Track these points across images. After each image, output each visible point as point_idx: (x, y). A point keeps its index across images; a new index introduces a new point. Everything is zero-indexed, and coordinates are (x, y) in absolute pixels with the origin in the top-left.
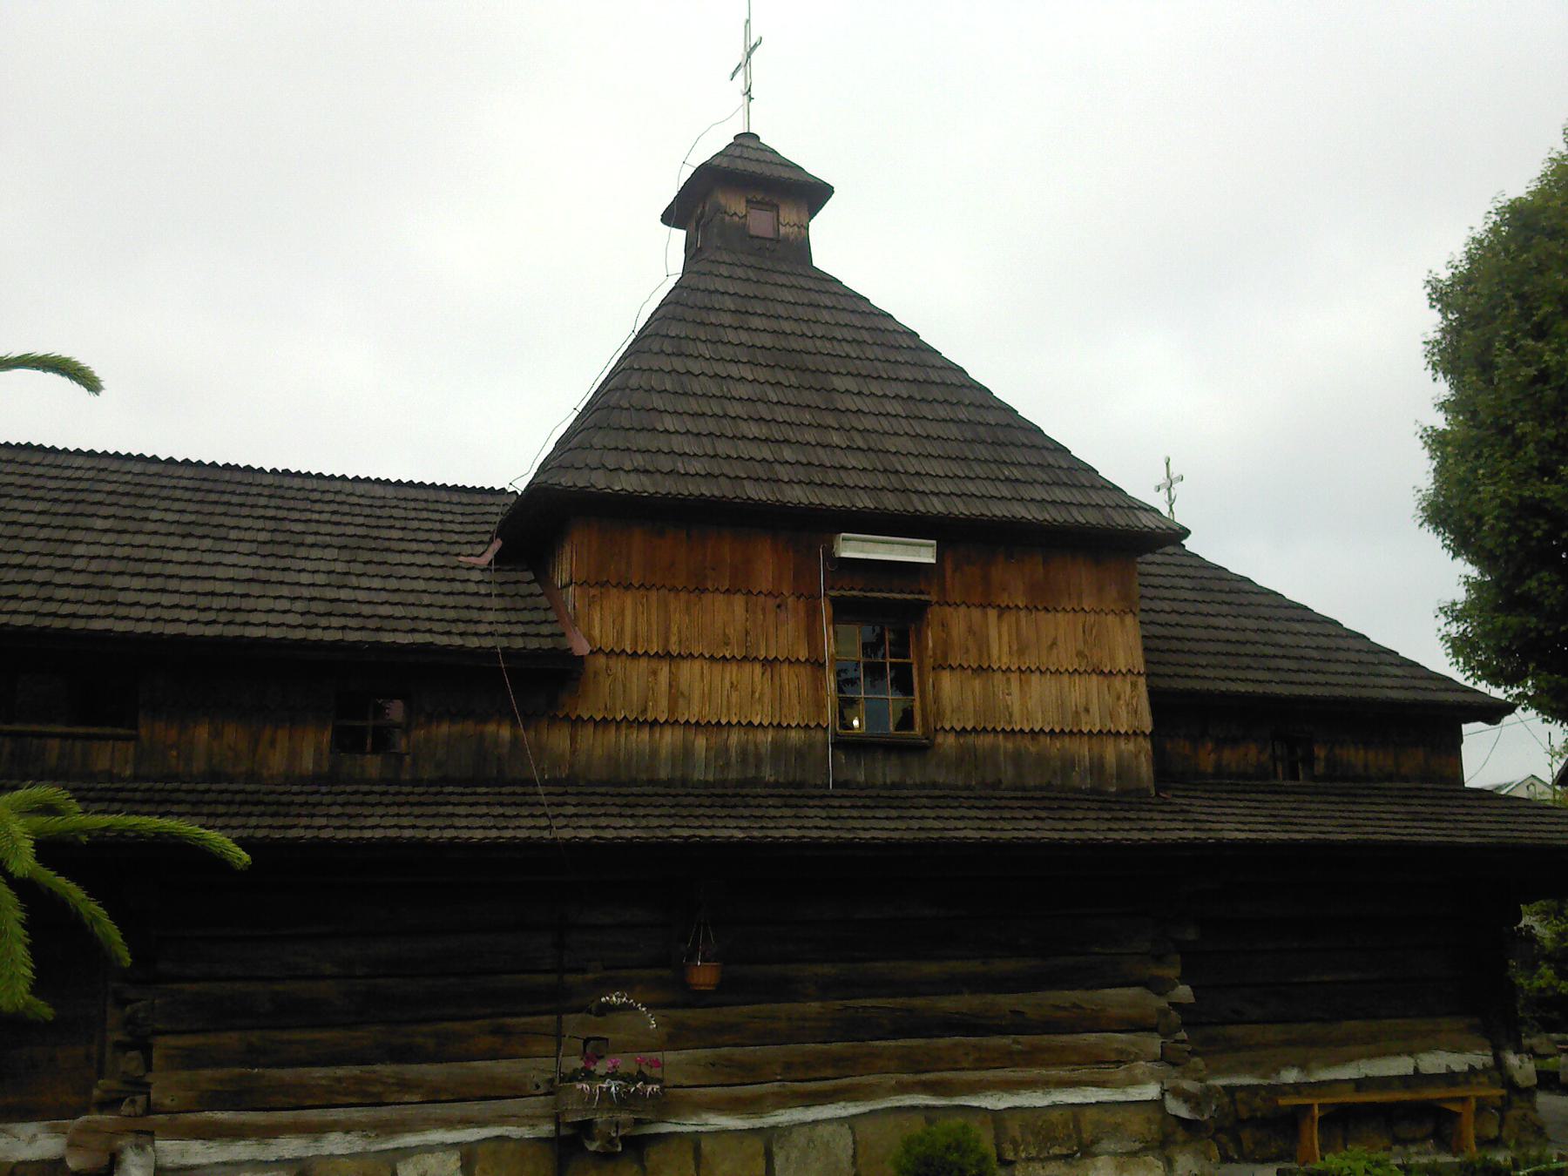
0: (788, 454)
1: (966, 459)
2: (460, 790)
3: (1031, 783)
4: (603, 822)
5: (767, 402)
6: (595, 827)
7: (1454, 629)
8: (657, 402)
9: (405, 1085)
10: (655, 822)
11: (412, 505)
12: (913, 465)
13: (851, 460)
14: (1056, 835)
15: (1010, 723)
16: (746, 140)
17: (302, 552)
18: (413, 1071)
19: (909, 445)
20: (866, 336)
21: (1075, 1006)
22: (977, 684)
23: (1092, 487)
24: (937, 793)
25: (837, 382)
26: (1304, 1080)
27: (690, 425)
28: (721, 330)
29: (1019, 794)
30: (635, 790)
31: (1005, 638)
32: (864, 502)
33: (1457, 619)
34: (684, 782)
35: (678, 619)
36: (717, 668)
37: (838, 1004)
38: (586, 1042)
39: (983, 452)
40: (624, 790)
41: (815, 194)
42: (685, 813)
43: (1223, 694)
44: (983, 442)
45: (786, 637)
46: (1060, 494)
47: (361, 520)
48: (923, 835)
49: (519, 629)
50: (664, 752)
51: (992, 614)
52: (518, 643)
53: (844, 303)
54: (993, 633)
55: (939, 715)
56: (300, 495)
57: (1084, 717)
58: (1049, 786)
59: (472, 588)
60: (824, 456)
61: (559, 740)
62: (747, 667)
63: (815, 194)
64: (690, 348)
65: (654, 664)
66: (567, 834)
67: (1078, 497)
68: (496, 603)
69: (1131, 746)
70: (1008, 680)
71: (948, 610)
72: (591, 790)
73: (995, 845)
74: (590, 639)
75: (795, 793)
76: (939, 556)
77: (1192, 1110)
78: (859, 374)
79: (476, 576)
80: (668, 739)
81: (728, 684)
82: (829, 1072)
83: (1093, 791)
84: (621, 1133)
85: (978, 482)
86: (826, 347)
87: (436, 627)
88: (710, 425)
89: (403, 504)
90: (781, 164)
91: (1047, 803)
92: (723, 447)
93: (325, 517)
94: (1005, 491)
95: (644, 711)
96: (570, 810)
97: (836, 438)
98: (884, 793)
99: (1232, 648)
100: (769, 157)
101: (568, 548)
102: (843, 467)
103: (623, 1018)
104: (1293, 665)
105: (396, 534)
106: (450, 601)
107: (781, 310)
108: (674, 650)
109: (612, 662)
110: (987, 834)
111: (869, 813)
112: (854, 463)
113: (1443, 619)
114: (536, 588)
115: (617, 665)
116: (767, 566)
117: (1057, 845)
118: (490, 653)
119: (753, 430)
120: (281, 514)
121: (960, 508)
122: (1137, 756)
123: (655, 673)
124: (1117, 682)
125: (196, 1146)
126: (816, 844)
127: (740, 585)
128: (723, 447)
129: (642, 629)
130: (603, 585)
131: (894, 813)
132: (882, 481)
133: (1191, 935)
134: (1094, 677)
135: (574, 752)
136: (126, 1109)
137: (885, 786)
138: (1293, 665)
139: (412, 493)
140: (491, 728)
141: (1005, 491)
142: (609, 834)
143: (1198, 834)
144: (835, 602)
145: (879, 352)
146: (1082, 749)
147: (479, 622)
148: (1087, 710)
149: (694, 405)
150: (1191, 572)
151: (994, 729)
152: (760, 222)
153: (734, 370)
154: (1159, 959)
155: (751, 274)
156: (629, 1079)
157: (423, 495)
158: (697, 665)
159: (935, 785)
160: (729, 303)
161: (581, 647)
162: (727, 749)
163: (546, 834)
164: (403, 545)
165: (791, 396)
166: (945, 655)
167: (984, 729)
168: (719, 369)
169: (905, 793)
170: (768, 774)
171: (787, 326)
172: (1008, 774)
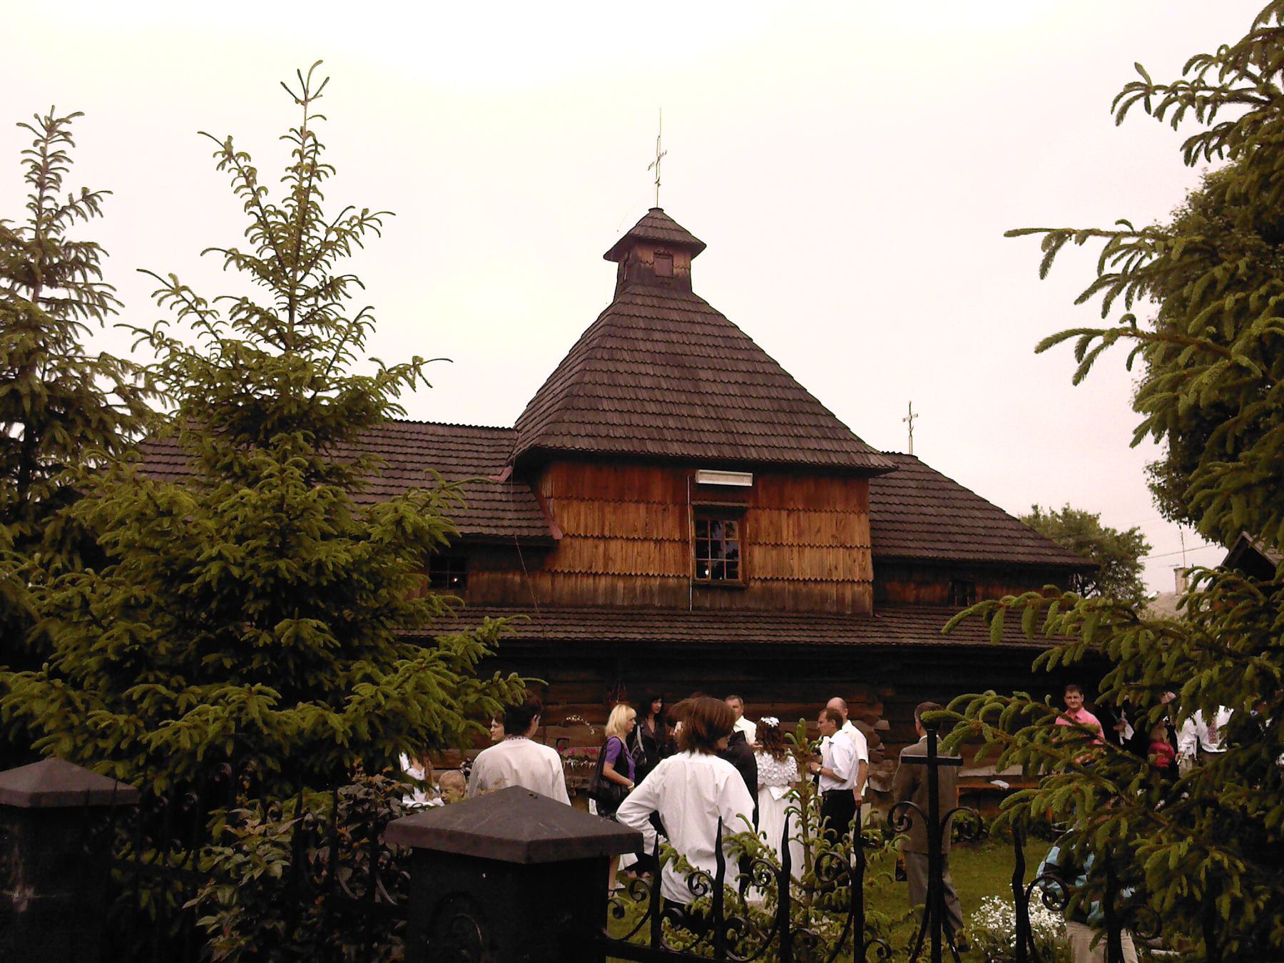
0: (671, 423)
1: (773, 423)
2: (495, 609)
4: (569, 628)
5: (660, 389)
6: (565, 632)
7: (1158, 481)
8: (600, 391)
10: (596, 629)
11: (460, 440)
12: (742, 428)
13: (706, 427)
14: (808, 640)
17: (406, 475)
19: (740, 414)
20: (721, 342)
22: (774, 553)
23: (845, 439)
24: (749, 613)
25: (703, 374)
27: (617, 405)
28: (636, 342)
29: (795, 615)
30: (585, 610)
31: (791, 528)
32: (713, 452)
33: (1158, 474)
34: (612, 606)
35: (610, 517)
36: (630, 544)
38: (558, 740)
39: (783, 418)
40: (579, 610)
41: (696, 247)
42: (611, 624)
43: (920, 558)
44: (784, 411)
45: (668, 527)
46: (826, 445)
47: (434, 452)
48: (736, 638)
49: (524, 523)
51: (784, 513)
52: (525, 532)
53: (710, 319)
55: (753, 570)
56: (399, 435)
57: (834, 572)
58: (812, 611)
59: (498, 497)
60: (691, 423)
61: (545, 583)
62: (646, 544)
63: (696, 247)
64: (618, 355)
65: (596, 542)
66: (551, 635)
67: (835, 446)
68: (512, 506)
69: (861, 589)
71: (759, 511)
72: (562, 610)
73: (775, 644)
74: (562, 528)
75: (671, 614)
77: (881, 787)
78: (715, 368)
79: (499, 488)
80: (603, 583)
83: (838, 613)
84: (576, 785)
85: (778, 438)
86: (697, 350)
87: (482, 522)
88: (628, 405)
89: (455, 440)
90: (676, 230)
91: (808, 621)
92: (636, 419)
93: (415, 450)
94: (794, 444)
95: (591, 568)
96: (552, 622)
97: (699, 412)
98: (719, 614)
99: (931, 528)
100: (668, 224)
101: (550, 478)
102: (702, 431)
103: (577, 729)
104: (966, 539)
105: (454, 461)
106: (487, 505)
107: (671, 326)
108: (607, 534)
109: (573, 541)
110: (771, 638)
111: (709, 625)
112: (708, 427)
113: (1149, 474)
114: (532, 496)
115: (576, 543)
117: (810, 645)
118: (510, 538)
119: (652, 408)
120: (392, 449)
121: (767, 455)
122: (864, 594)
123: (596, 547)
124: (855, 552)
126: (679, 642)
127: (643, 497)
128: (636, 419)
129: (590, 523)
130: (568, 498)
131: (723, 626)
132: (723, 438)
133: (889, 693)
134: (841, 549)
135: (553, 589)
137: (720, 609)
138: (966, 539)
139: (459, 432)
140: (510, 576)
141: (794, 444)
142: (573, 636)
143: (887, 640)
144: (695, 508)
145: (727, 353)
146: (832, 591)
147: (503, 519)
148: (836, 568)
149: (620, 393)
150: (918, 476)
152: (661, 267)
153: (643, 369)
154: (871, 705)
155: (655, 302)
156: (581, 759)
157: (465, 433)
158: (619, 543)
159: (748, 609)
160: (642, 324)
161: (558, 535)
162: (634, 589)
163: (541, 635)
164: (459, 469)
165: (675, 384)
166: (757, 536)
167: (777, 578)
168: (635, 368)
169: (731, 613)
170: (657, 603)
171: (674, 337)
172: (790, 604)
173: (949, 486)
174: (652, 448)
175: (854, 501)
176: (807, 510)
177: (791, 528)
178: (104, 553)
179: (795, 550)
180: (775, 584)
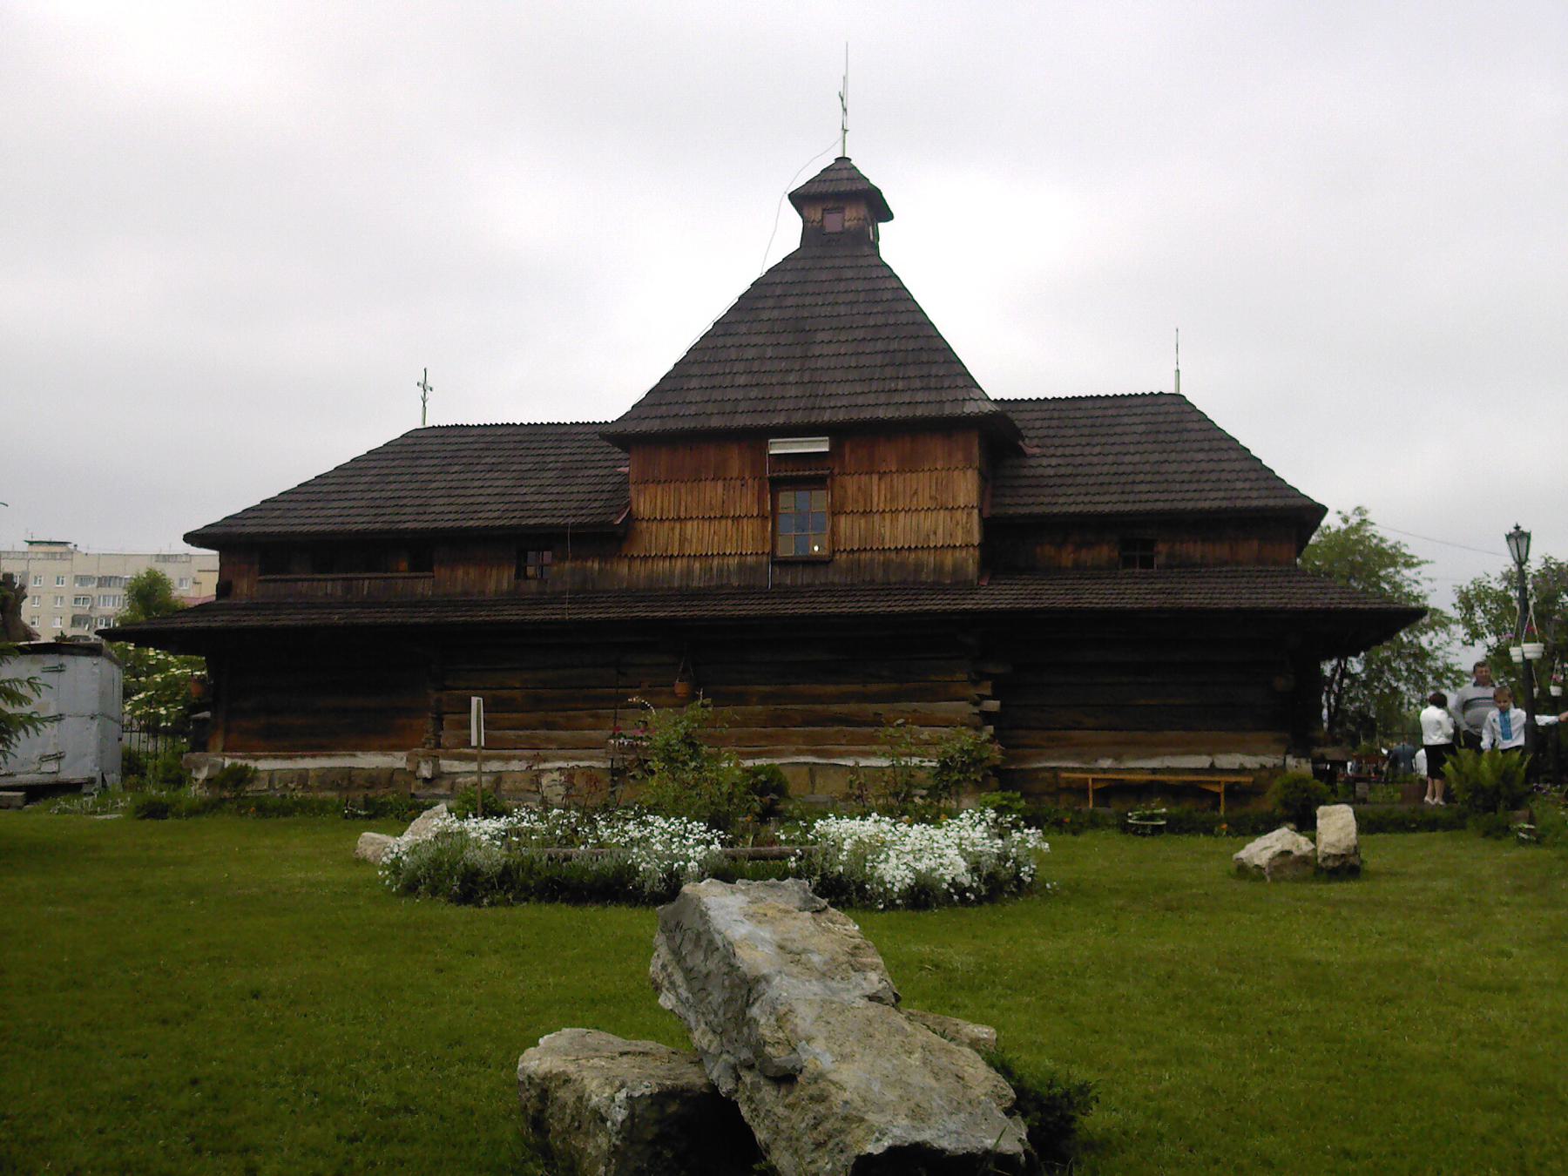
3: (893, 579)
9: (549, 740)
15: (882, 544)
16: (843, 160)
18: (555, 733)
21: (915, 711)
26: (1117, 766)
31: (883, 492)
32: (779, 420)
36: (707, 523)
37: (772, 708)
50: (677, 572)
51: (875, 478)
54: (875, 488)
57: (932, 537)
61: (623, 569)
62: (724, 522)
69: (964, 553)
70: (884, 518)
76: (831, 447)
80: (679, 565)
81: (712, 531)
82: (763, 743)
115: (654, 526)
116: (736, 461)
121: (841, 416)
123: (673, 529)
125: (456, 763)
136: (427, 746)
140: (589, 564)
146: (930, 559)
148: (935, 533)
151: (871, 548)
166: (842, 505)
167: (865, 549)
172: (879, 575)
173: (1202, 417)
174: (716, 422)
175: (960, 456)
176: (901, 471)
177: (883, 492)
178: (993, 687)
179: (888, 516)
180: (863, 556)
